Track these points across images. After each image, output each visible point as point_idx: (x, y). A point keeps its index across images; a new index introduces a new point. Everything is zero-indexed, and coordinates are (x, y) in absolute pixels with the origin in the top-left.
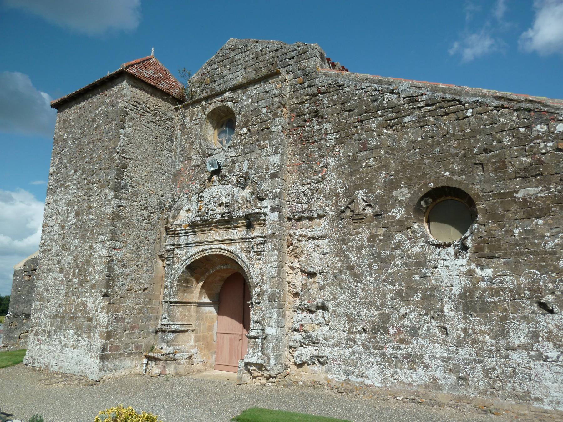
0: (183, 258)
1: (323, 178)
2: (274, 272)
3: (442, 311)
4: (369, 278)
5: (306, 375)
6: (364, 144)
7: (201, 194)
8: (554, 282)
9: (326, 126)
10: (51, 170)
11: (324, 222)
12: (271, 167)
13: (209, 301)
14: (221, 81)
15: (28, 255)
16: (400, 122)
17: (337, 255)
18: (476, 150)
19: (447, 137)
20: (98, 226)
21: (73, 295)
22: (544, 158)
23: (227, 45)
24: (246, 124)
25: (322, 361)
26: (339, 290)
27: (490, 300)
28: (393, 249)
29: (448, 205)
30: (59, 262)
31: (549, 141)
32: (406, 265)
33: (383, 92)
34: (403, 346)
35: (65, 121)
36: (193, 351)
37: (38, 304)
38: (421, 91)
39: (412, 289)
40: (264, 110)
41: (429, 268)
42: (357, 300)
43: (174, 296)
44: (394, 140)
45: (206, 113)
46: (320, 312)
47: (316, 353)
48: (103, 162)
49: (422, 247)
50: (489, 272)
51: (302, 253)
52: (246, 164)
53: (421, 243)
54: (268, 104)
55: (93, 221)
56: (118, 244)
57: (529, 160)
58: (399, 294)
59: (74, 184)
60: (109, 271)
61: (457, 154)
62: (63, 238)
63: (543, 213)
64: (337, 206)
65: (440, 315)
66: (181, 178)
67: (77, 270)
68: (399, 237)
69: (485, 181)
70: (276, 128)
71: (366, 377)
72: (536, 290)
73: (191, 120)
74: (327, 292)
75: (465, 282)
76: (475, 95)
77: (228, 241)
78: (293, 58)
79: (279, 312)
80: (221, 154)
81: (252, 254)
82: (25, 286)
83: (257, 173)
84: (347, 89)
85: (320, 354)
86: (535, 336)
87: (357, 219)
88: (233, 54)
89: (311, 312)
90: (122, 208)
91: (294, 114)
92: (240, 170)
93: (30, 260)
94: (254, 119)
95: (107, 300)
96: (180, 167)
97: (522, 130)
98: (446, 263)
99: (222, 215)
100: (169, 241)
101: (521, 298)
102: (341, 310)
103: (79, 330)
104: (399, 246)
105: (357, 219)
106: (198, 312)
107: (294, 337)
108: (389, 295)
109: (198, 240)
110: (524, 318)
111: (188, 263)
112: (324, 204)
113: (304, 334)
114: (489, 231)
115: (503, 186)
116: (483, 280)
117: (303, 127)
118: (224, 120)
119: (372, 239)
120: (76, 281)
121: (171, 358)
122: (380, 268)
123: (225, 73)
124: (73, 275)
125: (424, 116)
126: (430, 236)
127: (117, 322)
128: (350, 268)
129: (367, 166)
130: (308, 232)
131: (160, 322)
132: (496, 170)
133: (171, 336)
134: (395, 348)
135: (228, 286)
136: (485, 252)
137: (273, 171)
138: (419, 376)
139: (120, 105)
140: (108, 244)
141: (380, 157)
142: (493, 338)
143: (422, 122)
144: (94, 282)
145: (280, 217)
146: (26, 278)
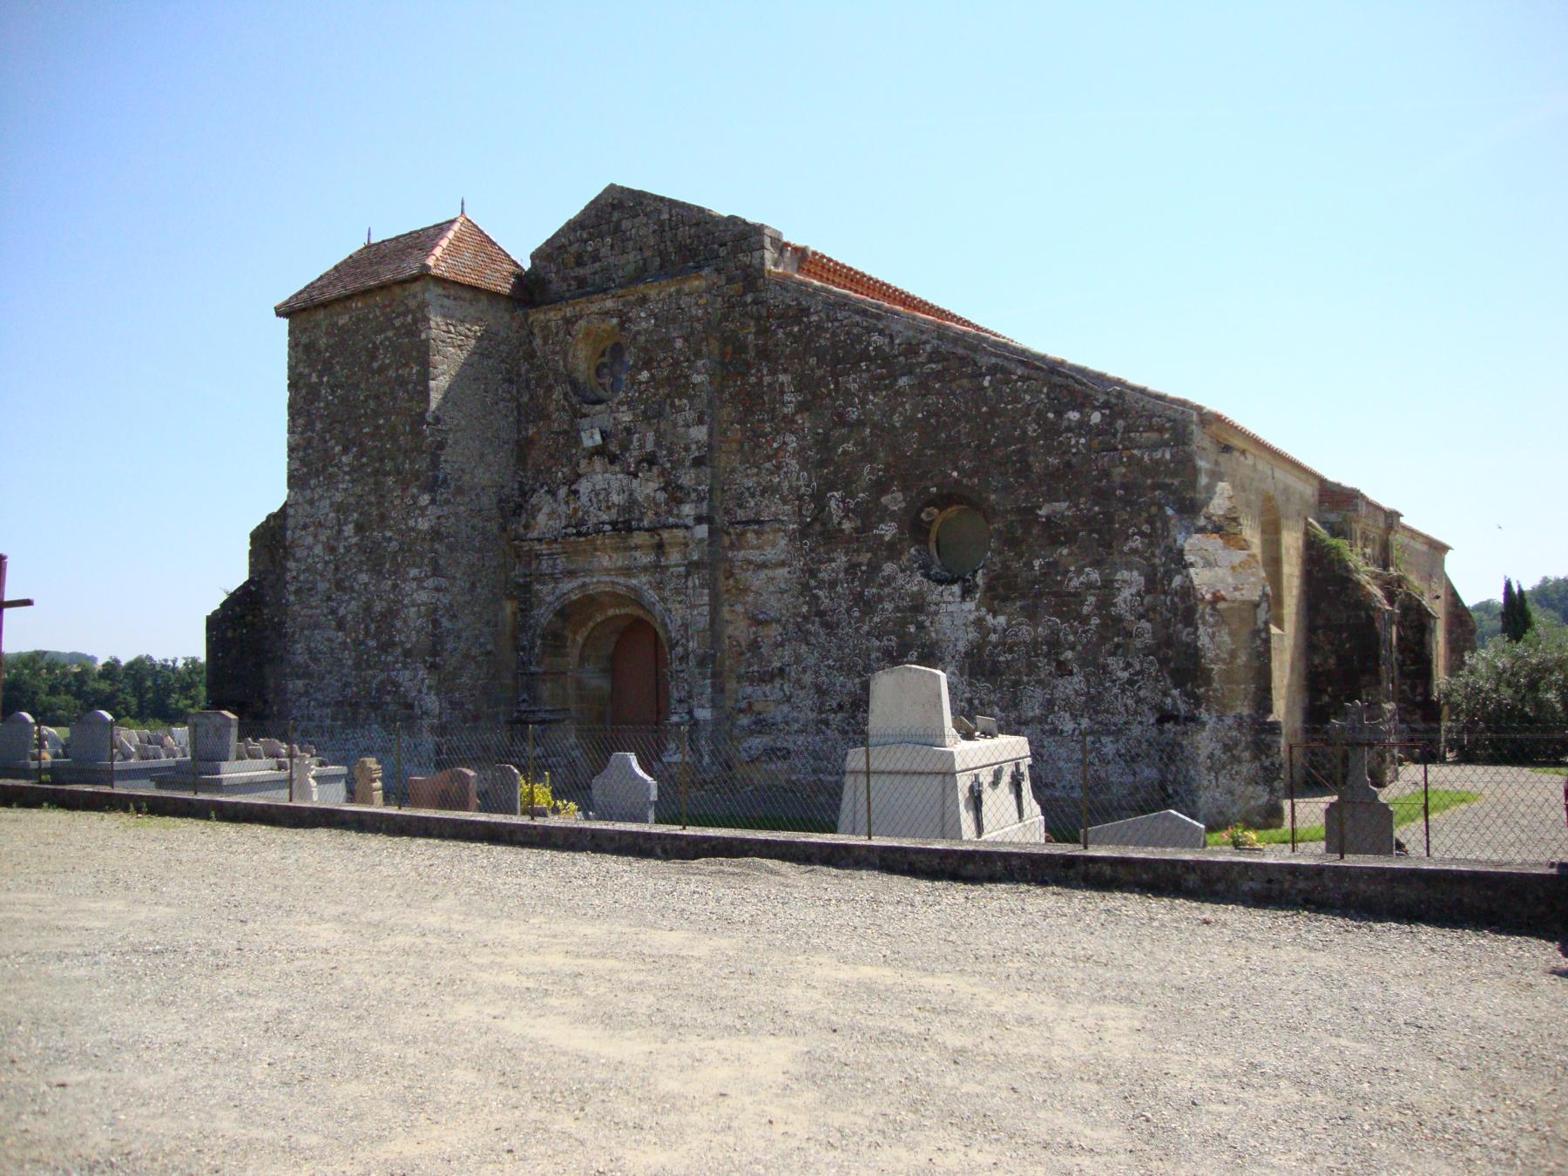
2: (703, 622)
6: (840, 416)
8: (1075, 633)
9: (782, 378)
12: (694, 447)
14: (597, 265)
17: (801, 594)
21: (370, 667)
22: (1074, 460)
26: (804, 647)
28: (881, 586)
30: (333, 612)
32: (897, 609)
33: (869, 330)
36: (576, 753)
37: (300, 683)
38: (924, 337)
40: (679, 344)
42: (831, 662)
50: (1002, 619)
51: (746, 590)
52: (651, 436)
56: (444, 583)
60: (434, 627)
61: (968, 445)
62: (337, 569)
63: (1070, 538)
64: (801, 515)
67: (373, 626)
68: (889, 568)
72: (1055, 644)
73: (545, 343)
75: (973, 635)
76: (996, 355)
77: (627, 571)
79: (713, 685)
86: (1049, 704)
87: (831, 537)
92: (642, 447)
98: (950, 608)
101: (1037, 655)
103: (387, 721)
104: (889, 580)
105: (831, 537)
108: (873, 656)
110: (1040, 682)
114: (1003, 563)
116: (995, 631)
119: (852, 568)
129: (845, 453)
140: (430, 583)
142: (1002, 710)
143: (923, 387)
145: (711, 532)
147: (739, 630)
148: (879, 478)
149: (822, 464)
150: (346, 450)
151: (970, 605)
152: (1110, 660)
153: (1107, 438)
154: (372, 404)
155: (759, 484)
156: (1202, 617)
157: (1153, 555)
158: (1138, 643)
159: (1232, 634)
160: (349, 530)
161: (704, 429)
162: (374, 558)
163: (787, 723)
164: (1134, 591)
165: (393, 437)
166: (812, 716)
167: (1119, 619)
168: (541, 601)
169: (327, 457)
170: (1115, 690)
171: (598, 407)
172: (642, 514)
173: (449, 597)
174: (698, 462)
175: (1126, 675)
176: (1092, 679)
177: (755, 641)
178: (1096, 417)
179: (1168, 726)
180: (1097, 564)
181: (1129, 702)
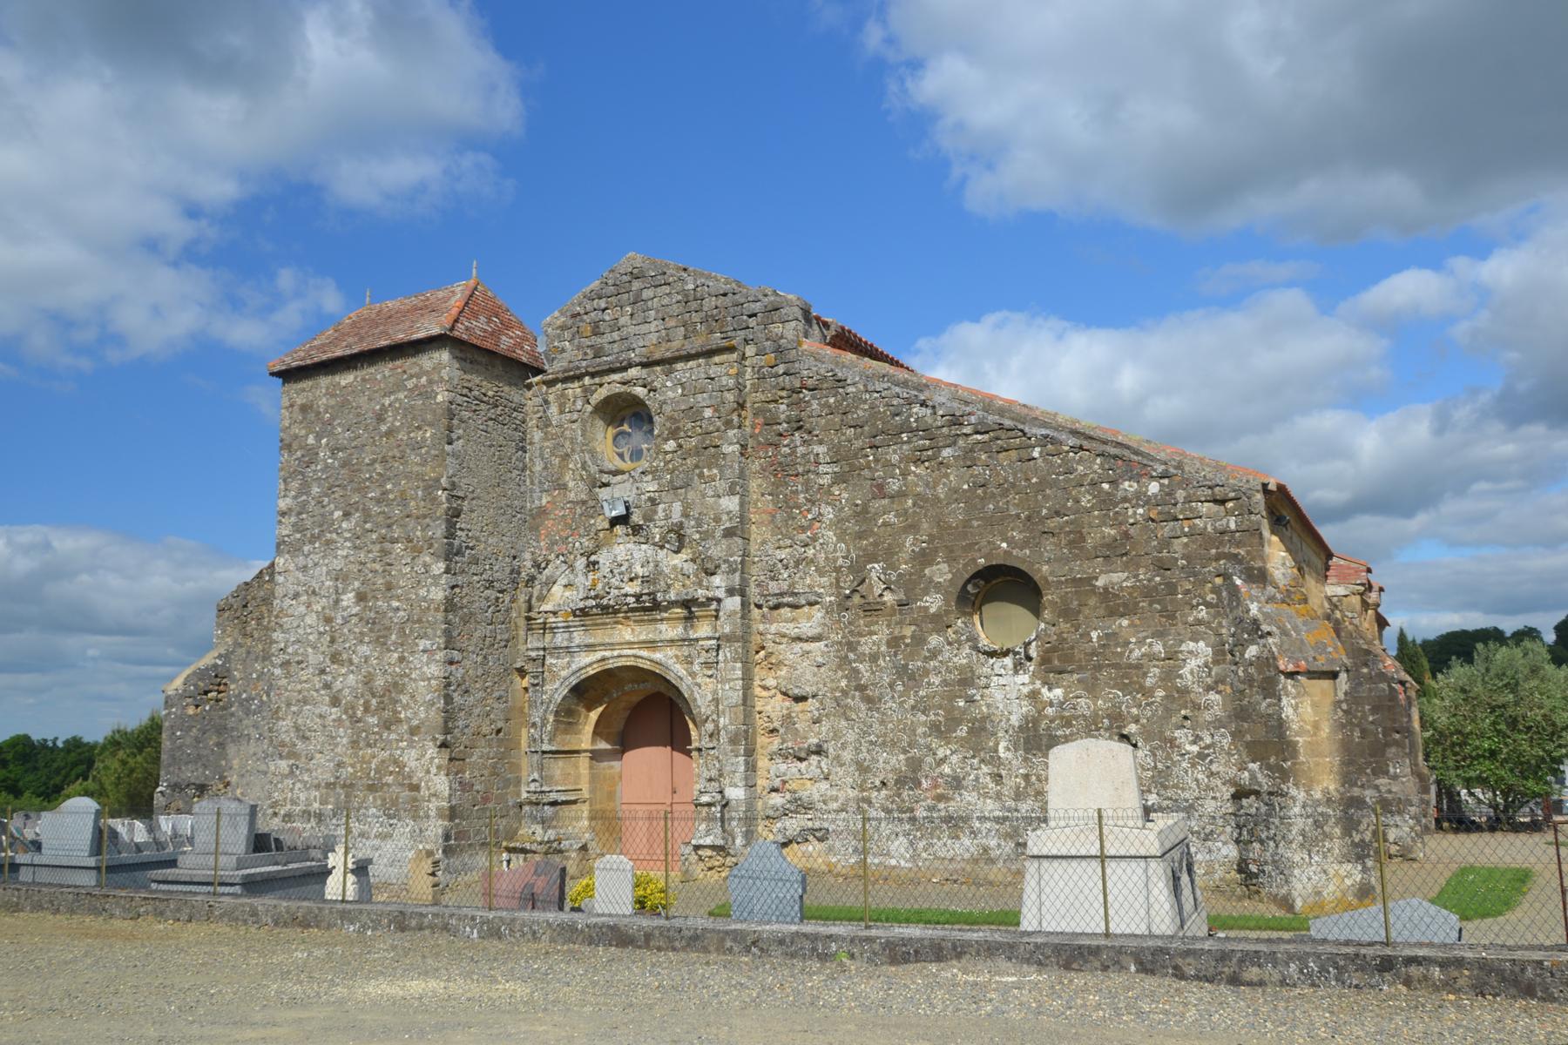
0: (564, 673)
1: (814, 539)
2: (737, 697)
3: (996, 751)
4: (890, 704)
6: (881, 487)
7: (593, 558)
9: (820, 449)
10: (283, 504)
11: (818, 614)
12: (725, 517)
13: (609, 747)
14: (616, 335)
15: (188, 665)
16: (935, 457)
17: (840, 667)
18: (1044, 511)
19: (1005, 489)
20: (415, 622)
21: (369, 745)
22: (1132, 531)
23: (624, 265)
24: (674, 434)
25: (822, 836)
26: (844, 723)
27: (1059, 733)
31: (1138, 506)
32: (945, 683)
34: (941, 806)
35: (304, 409)
38: (968, 409)
39: (953, 719)
40: (708, 413)
41: (978, 688)
42: (873, 738)
43: (550, 741)
44: (927, 485)
45: (593, 402)
46: (814, 759)
47: (810, 824)
48: (412, 503)
49: (968, 656)
50: (1058, 692)
51: (780, 663)
52: (677, 508)
53: (966, 650)
54: (713, 402)
55: (402, 613)
56: (456, 655)
57: (1113, 532)
58: (935, 728)
59: (346, 539)
60: (446, 703)
61: (1018, 516)
62: (333, 641)
63: (1128, 609)
64: (838, 586)
65: (994, 760)
66: (549, 523)
67: (374, 702)
68: (934, 640)
69: (1055, 560)
70: (731, 449)
71: (888, 854)
73: (562, 412)
74: (825, 727)
77: (651, 645)
78: (755, 315)
79: (747, 763)
80: (628, 485)
81: (696, 668)
82: (190, 728)
83: (699, 525)
84: (851, 389)
85: (817, 825)
87: (872, 609)
88: (636, 285)
89: (801, 760)
90: (457, 590)
91: (760, 420)
92: (667, 517)
93: (194, 673)
94: (689, 425)
95: (446, 754)
96: (544, 501)
97: (1106, 486)
98: (1002, 681)
99: (638, 597)
100: (534, 642)
102: (847, 755)
104: (934, 654)
105: (872, 609)
106: (591, 768)
107: (772, 802)
108: (920, 730)
109: (592, 641)
111: (574, 681)
112: (815, 582)
113: (788, 796)
115: (1079, 569)
116: (1051, 704)
117: (776, 446)
118: (626, 412)
119: (894, 642)
120: (373, 720)
122: (907, 688)
123: (622, 321)
124: (367, 709)
125: (972, 450)
126: (983, 636)
127: (463, 790)
128: (861, 688)
129: (885, 524)
130: (791, 629)
131: (524, 789)
132: (1071, 544)
133: (548, 810)
134: (931, 809)
136: (1054, 662)
137: (728, 525)
138: (965, 846)
139: (440, 398)
141: (906, 511)
144: (415, 722)
146: (191, 711)
147: (772, 706)
148: (923, 549)
149: (860, 536)
150: (347, 515)
151: (1024, 678)
152: (1177, 733)
153: (1166, 508)
154: (379, 468)
155: (793, 556)
156: (1285, 688)
157: (1220, 624)
158: (1208, 716)
159: (1314, 705)
160: (348, 599)
161: (736, 499)
162: (378, 630)
163: (825, 802)
164: (1200, 661)
165: (403, 500)
166: (852, 794)
167: (1184, 691)
168: (555, 676)
169: (325, 523)
170: (1184, 765)
171: (619, 478)
172: (669, 586)
173: (461, 671)
174: (729, 533)
175: (1195, 749)
176: (1159, 753)
177: (789, 716)
178: (1154, 487)
179: (1245, 802)
180: (1160, 635)
181: (1200, 776)
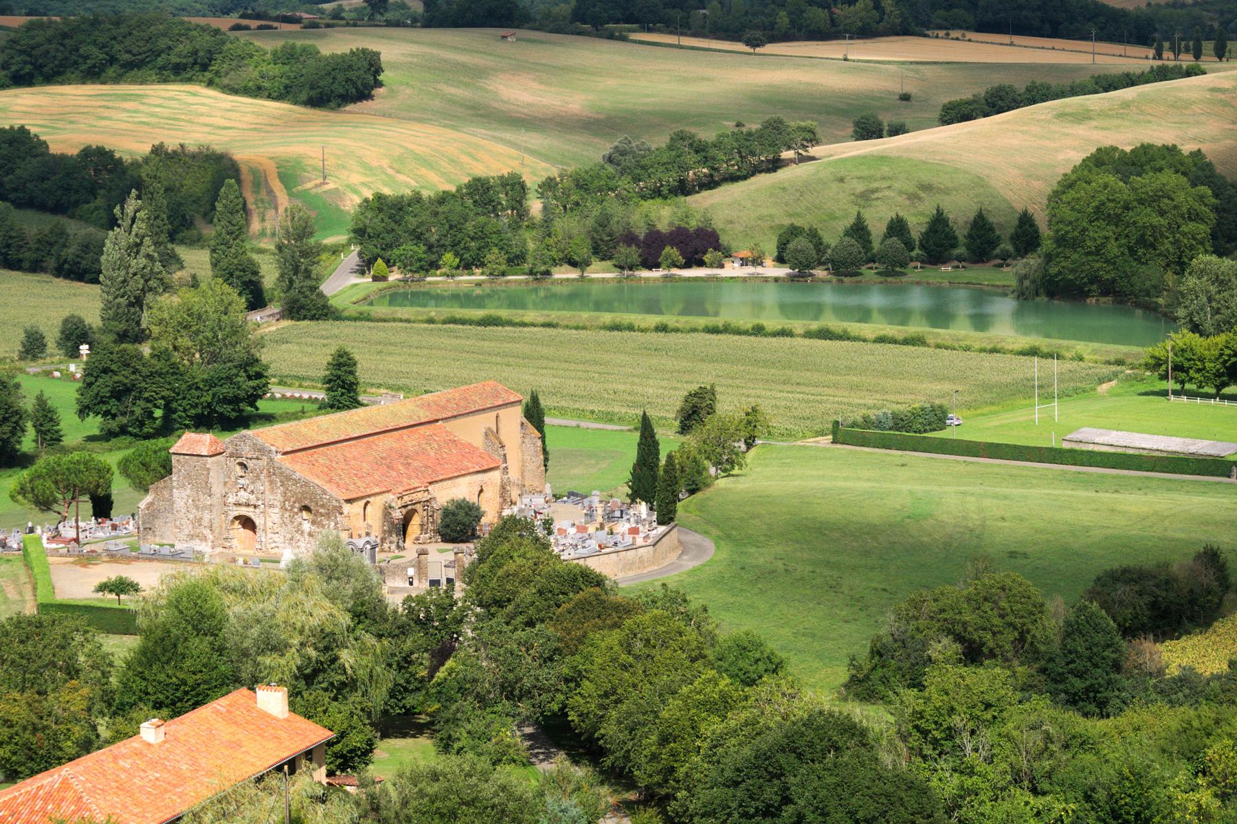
5: (273, 551)
29: (306, 508)
121: (230, 547)
135: (248, 523)
